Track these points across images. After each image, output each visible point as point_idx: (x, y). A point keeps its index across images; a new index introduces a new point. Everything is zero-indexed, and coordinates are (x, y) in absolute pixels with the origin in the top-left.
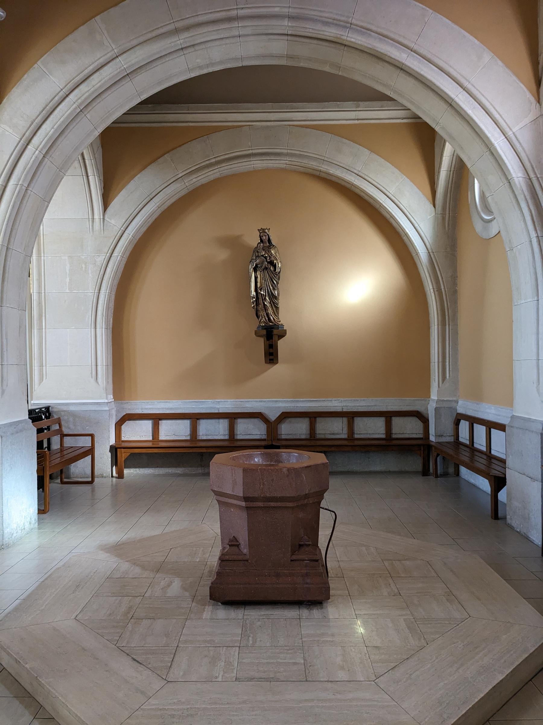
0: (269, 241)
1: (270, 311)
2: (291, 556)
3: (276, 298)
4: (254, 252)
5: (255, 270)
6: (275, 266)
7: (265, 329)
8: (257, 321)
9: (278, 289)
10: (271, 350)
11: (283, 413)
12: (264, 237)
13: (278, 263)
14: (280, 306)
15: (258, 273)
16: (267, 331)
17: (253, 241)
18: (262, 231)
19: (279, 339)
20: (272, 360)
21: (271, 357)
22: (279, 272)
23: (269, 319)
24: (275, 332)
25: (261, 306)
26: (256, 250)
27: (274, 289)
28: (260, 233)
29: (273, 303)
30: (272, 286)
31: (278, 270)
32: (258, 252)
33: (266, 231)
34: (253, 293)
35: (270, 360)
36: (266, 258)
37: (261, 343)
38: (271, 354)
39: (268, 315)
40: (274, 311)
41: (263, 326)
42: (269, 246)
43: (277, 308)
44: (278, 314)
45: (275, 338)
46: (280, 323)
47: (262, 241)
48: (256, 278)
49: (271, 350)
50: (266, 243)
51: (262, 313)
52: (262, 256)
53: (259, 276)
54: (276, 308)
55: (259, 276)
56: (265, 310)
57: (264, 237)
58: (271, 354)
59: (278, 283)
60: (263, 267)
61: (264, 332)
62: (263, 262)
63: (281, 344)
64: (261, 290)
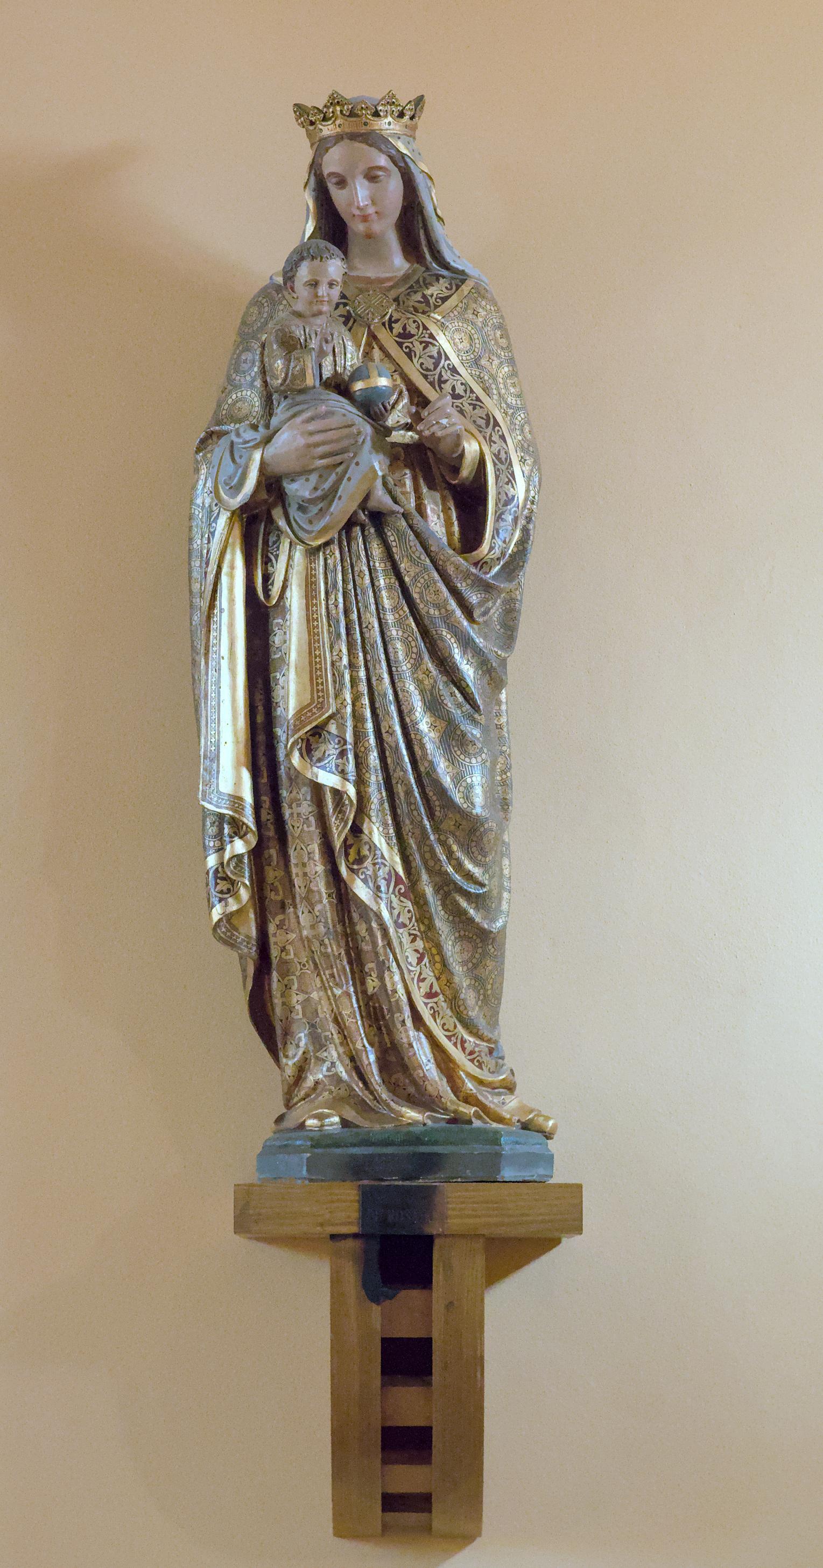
0: (413, 226)
1: (406, 974)
2: (392, 332)
3: (473, 834)
4: (246, 336)
5: (257, 525)
6: (470, 502)
7: (356, 1169)
8: (261, 1076)
9: (495, 735)
10: (409, 1404)
11: (480, 1535)
12: (362, 192)
13: (503, 461)
14: (517, 917)
15: (290, 566)
16: (368, 1198)
17: (254, 224)
18: (342, 123)
19: (494, 1275)
20: (421, 1502)
21: (408, 1478)
22: (514, 564)
23: (394, 1060)
24: (459, 1208)
25: (308, 922)
26: (270, 321)
27: (454, 740)
28: (321, 147)
29: (446, 887)
30: (434, 705)
31: (497, 539)
32: (290, 345)
33: (387, 125)
34: (231, 779)
35: (391, 1502)
36: (372, 408)
37: (295, 1321)
38: (406, 1443)
39: (376, 1014)
40: (444, 969)
41: (321, 1142)
42: (413, 284)
43: (481, 942)
44: (490, 998)
45: (452, 1266)
46: (509, 1105)
47: (334, 228)
48: (260, 618)
49: (409, 1404)
50: (379, 237)
51: (317, 996)
52: (340, 386)
53: (295, 599)
54: (464, 923)
55: (295, 599)
56: (356, 959)
57: (362, 192)
58: (406, 1443)
59: (494, 675)
60: (343, 507)
61: (342, 1206)
62: (339, 460)
63: (521, 1332)
64: (311, 742)
